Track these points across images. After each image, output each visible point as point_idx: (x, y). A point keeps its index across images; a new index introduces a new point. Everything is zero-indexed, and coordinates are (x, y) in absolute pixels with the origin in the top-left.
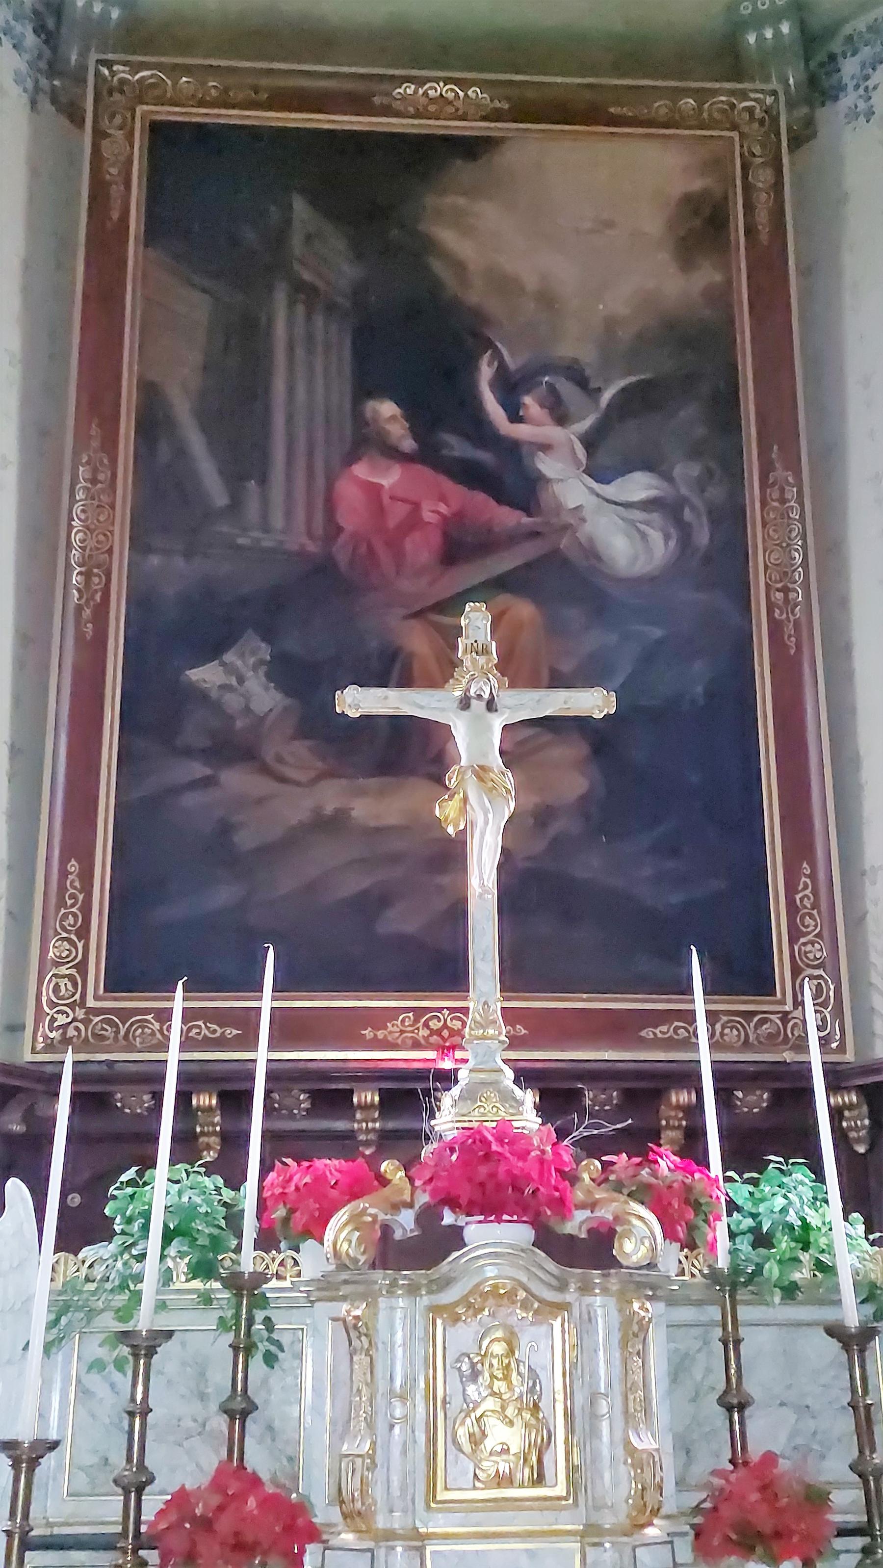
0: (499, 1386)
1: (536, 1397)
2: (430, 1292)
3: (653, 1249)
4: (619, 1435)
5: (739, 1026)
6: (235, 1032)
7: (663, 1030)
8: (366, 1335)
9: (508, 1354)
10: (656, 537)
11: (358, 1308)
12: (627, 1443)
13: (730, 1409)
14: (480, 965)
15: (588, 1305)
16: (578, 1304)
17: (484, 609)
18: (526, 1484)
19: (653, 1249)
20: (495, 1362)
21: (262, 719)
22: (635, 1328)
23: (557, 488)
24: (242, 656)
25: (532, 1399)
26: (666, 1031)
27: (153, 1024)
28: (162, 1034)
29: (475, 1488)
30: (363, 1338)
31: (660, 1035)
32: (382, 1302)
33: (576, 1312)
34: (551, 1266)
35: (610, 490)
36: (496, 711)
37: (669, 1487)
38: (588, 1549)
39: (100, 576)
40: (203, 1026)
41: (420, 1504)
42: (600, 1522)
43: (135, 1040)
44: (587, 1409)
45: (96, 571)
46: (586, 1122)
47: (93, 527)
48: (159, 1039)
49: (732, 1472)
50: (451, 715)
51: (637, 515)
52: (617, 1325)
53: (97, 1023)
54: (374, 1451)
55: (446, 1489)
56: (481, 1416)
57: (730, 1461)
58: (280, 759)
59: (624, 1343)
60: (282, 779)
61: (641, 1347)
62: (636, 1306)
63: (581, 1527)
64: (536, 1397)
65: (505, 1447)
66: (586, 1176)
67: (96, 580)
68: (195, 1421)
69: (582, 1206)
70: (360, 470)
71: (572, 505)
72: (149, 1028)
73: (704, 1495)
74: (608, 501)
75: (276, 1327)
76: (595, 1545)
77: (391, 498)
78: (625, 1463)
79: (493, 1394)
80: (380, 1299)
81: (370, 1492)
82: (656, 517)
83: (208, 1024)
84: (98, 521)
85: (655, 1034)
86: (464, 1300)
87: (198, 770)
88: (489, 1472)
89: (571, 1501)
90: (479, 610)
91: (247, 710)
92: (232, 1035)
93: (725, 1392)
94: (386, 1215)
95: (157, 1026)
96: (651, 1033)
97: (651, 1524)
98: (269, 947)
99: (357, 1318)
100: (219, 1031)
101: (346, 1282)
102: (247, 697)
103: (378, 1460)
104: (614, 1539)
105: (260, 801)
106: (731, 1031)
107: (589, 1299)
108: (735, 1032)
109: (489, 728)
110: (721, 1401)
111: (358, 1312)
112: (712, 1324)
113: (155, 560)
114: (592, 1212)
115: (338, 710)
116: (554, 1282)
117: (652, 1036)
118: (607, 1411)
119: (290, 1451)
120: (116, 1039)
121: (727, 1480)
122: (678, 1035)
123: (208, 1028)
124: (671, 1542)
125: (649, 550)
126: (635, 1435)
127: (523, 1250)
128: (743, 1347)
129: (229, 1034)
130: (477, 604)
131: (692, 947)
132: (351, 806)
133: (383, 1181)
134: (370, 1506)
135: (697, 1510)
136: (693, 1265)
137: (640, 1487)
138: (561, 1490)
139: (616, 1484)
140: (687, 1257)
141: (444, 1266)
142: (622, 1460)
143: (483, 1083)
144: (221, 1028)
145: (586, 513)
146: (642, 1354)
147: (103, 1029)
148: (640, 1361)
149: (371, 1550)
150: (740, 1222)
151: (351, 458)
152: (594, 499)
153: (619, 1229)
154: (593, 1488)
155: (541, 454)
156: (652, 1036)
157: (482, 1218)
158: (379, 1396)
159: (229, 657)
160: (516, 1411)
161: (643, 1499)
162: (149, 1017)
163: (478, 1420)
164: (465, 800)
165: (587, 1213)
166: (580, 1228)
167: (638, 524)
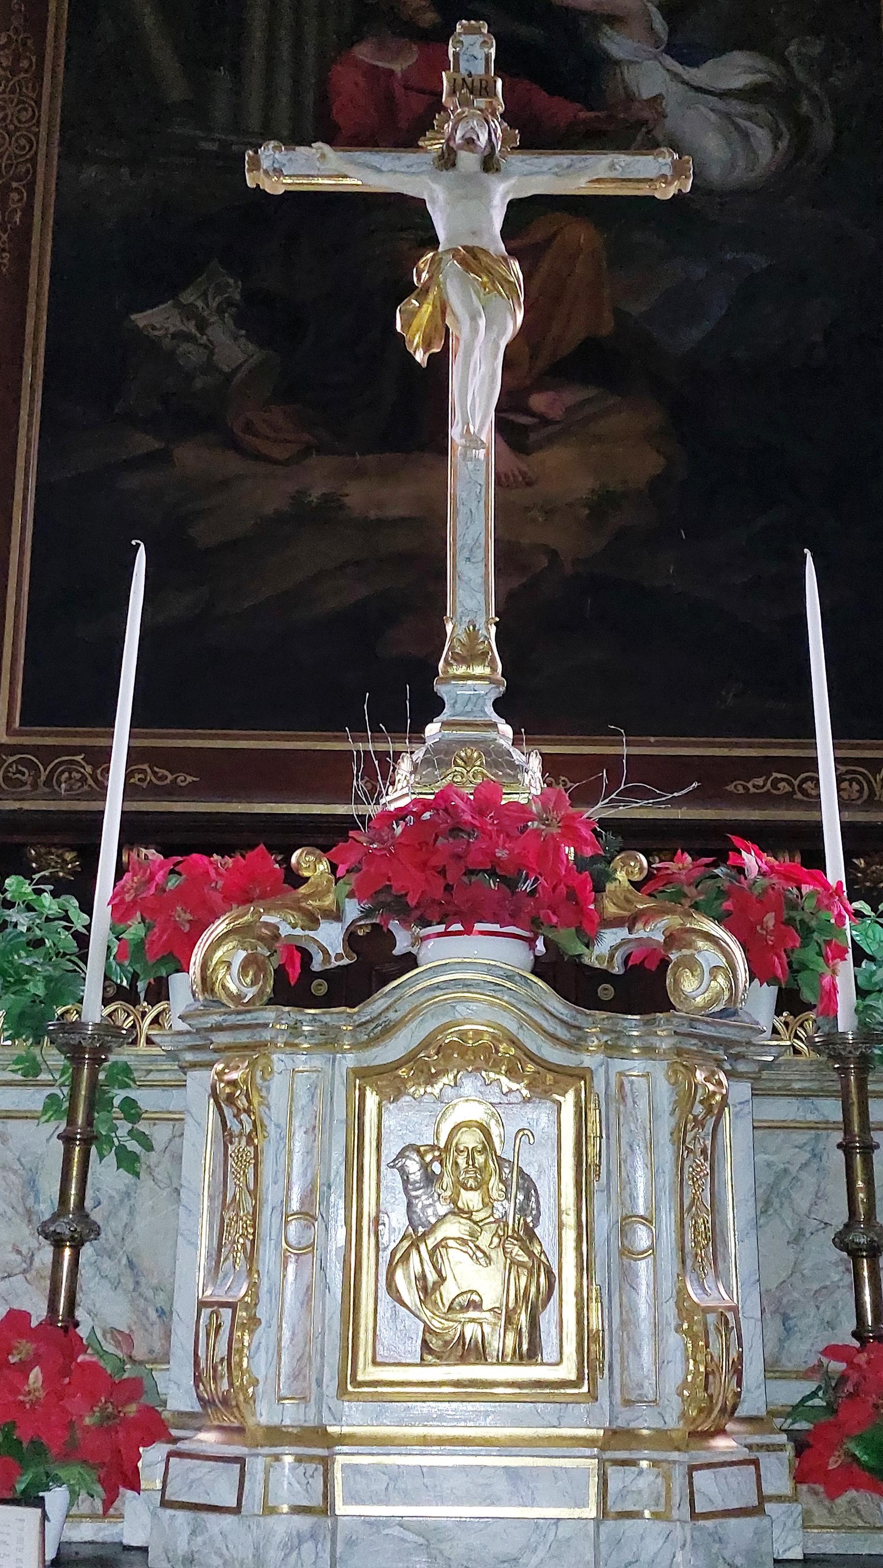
0: (471, 1199)
1: (529, 1219)
2: (358, 1046)
3: (733, 989)
4: (668, 1286)
5: (861, 778)
6: (190, 779)
7: (756, 783)
8: (248, 1111)
9: (484, 1147)
10: (761, 136)
11: (237, 1068)
12: (681, 1294)
13: (854, 1253)
14: (462, 566)
15: (621, 1074)
16: (602, 1070)
17: (485, 31)
18: (509, 1360)
19: (733, 989)
20: (462, 1161)
21: (229, 377)
22: (699, 1109)
23: (629, 75)
24: (204, 295)
25: (522, 1221)
26: (761, 784)
27: (83, 767)
28: (96, 781)
29: (423, 1363)
30: (244, 1116)
31: (753, 790)
32: (279, 1060)
33: (599, 1085)
34: (556, 1004)
35: (699, 75)
36: (497, 170)
37: (753, 1371)
38: (611, 1470)
39: (21, 193)
40: (149, 770)
41: (331, 1387)
42: (633, 1425)
43: (59, 787)
44: (616, 1243)
45: (14, 185)
46: (622, 787)
47: (11, 127)
48: (90, 786)
49: (859, 1351)
50: (426, 179)
51: (737, 107)
52: (668, 1108)
53: (10, 765)
54: (256, 1296)
55: (375, 1363)
56: (436, 1247)
57: (855, 1334)
58: (249, 427)
59: (679, 1137)
60: (258, 457)
61: (708, 1143)
62: (700, 1076)
63: (601, 1432)
64: (529, 1219)
65: (475, 1297)
66: (621, 875)
67: (15, 196)
68: (19, 1252)
69: (616, 922)
70: (364, 52)
71: (646, 94)
72: (79, 772)
73: (809, 1387)
74: (698, 89)
75: (143, 1116)
76: (624, 1463)
77: (406, 88)
78: (678, 1329)
79: (458, 1212)
80: (275, 1057)
81: (245, 1364)
82: (759, 109)
83: (156, 769)
84: (20, 121)
85: (746, 788)
86: (410, 1058)
87: (147, 443)
88: (448, 1338)
89: (585, 1389)
90: (477, 31)
91: (209, 367)
92: (187, 782)
93: (846, 1226)
94: (294, 928)
95: (89, 769)
96: (740, 788)
97: (721, 1432)
98: (138, 545)
99: (233, 1083)
100: (170, 777)
101: (219, 1028)
102: (210, 348)
103: (262, 1312)
104: (656, 1455)
105: (225, 484)
106: (851, 785)
107: (619, 1065)
108: (856, 787)
109: (484, 196)
110: (841, 1242)
111: (234, 1075)
112: (827, 1126)
113: (91, 173)
114: (630, 932)
115: (251, 184)
116: (562, 1032)
117: (742, 791)
118: (649, 1243)
119: (161, 1298)
120: (35, 786)
121: (851, 1364)
122: (779, 789)
123: (155, 773)
124: (755, 1463)
125: (751, 151)
126: (695, 1283)
127: (509, 978)
128: (877, 1156)
129: (182, 781)
130: (473, 22)
131: (806, 550)
132: (346, 491)
133: (295, 880)
134: (243, 1389)
135: (796, 1411)
136: (797, 1037)
137: (702, 1369)
138: (567, 1371)
139: (660, 1363)
140: (786, 1024)
141: (377, 1004)
142: (673, 1324)
143: (463, 743)
144: (172, 775)
145: (670, 106)
146: (711, 1155)
147: (19, 772)
148: (707, 1164)
149: (240, 1460)
150: (873, 973)
151: (352, 38)
152: (676, 87)
153: (674, 956)
154: (623, 1369)
155: (606, 29)
156: (742, 791)
157: (441, 928)
158: (267, 1211)
159: (188, 297)
160: (496, 1240)
161: (706, 1389)
162: (79, 758)
163: (432, 1253)
164: (443, 308)
165: (622, 933)
166: (612, 957)
167: (739, 121)
